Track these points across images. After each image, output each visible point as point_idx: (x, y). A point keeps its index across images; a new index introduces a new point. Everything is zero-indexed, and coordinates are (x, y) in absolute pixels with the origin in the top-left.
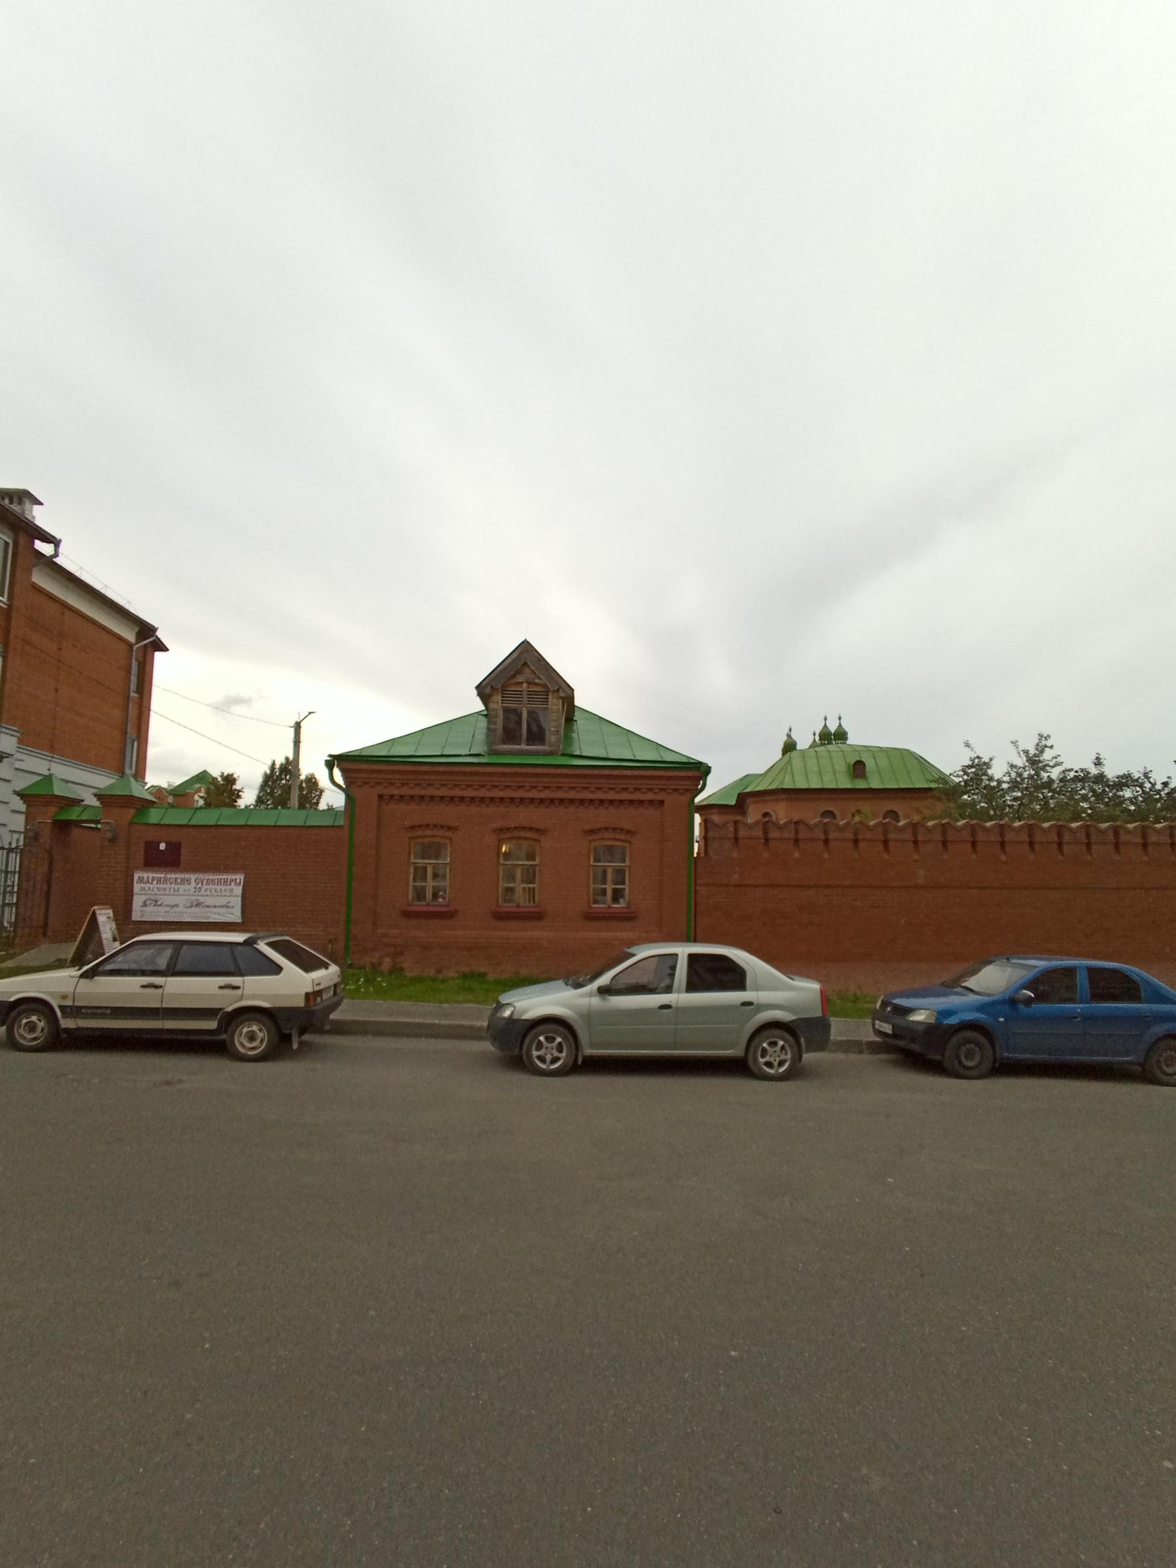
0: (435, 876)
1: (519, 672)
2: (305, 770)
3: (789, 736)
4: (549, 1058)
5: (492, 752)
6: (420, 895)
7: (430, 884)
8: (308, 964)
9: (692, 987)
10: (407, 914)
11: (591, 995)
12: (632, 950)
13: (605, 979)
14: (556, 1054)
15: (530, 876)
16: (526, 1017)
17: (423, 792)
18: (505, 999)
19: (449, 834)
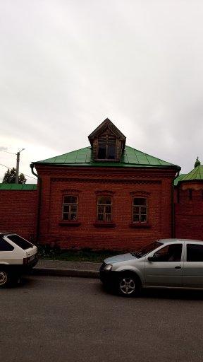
0: (72, 210)
1: (105, 131)
2: (21, 171)
3: (197, 160)
4: (127, 289)
5: (94, 162)
6: (66, 216)
7: (70, 213)
8: (25, 246)
9: (189, 260)
10: (62, 225)
11: (145, 261)
12: (161, 241)
13: (151, 254)
14: (130, 287)
15: (109, 210)
16: (117, 270)
17: (68, 177)
18: (107, 261)
19: (77, 193)
